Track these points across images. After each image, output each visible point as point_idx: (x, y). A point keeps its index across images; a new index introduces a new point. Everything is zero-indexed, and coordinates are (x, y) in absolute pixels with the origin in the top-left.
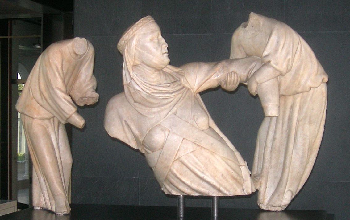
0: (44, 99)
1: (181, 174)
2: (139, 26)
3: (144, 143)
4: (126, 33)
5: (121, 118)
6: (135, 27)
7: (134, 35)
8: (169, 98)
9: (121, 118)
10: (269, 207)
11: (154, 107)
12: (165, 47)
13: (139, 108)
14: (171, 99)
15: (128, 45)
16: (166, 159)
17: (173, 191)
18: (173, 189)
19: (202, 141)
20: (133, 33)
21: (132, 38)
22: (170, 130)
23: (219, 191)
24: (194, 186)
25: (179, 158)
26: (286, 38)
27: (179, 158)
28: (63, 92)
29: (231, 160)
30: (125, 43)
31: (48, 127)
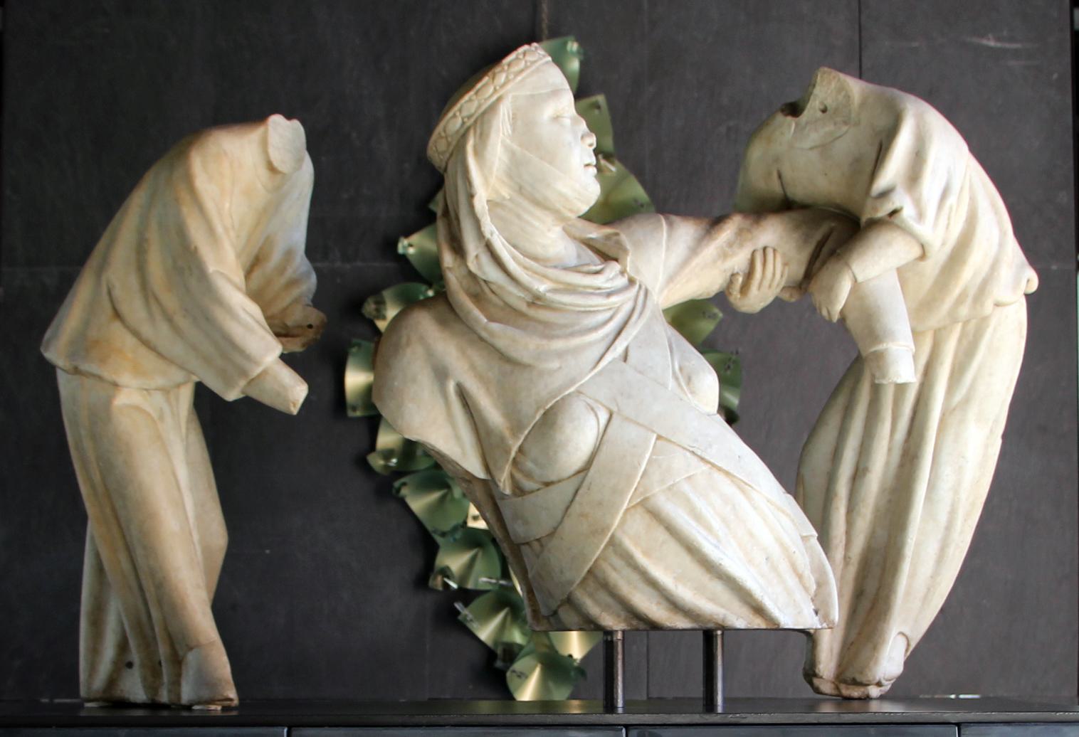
0: (158, 317)
1: (647, 553)
2: (515, 69)
3: (521, 459)
4: (472, 93)
5: (441, 374)
6: (500, 72)
7: (499, 99)
8: (598, 311)
9: (441, 374)
10: (842, 687)
11: (558, 337)
12: (591, 145)
13: (502, 334)
14: (608, 315)
15: (478, 131)
16: (600, 504)
17: (604, 614)
18: (606, 608)
19: (710, 446)
20: (495, 90)
21: (493, 108)
22: (615, 409)
23: (759, 610)
24: (686, 594)
25: (646, 499)
26: (686, 262)
27: (646, 499)
28: (239, 289)
29: (788, 515)
30: (463, 123)
31: (161, 418)
